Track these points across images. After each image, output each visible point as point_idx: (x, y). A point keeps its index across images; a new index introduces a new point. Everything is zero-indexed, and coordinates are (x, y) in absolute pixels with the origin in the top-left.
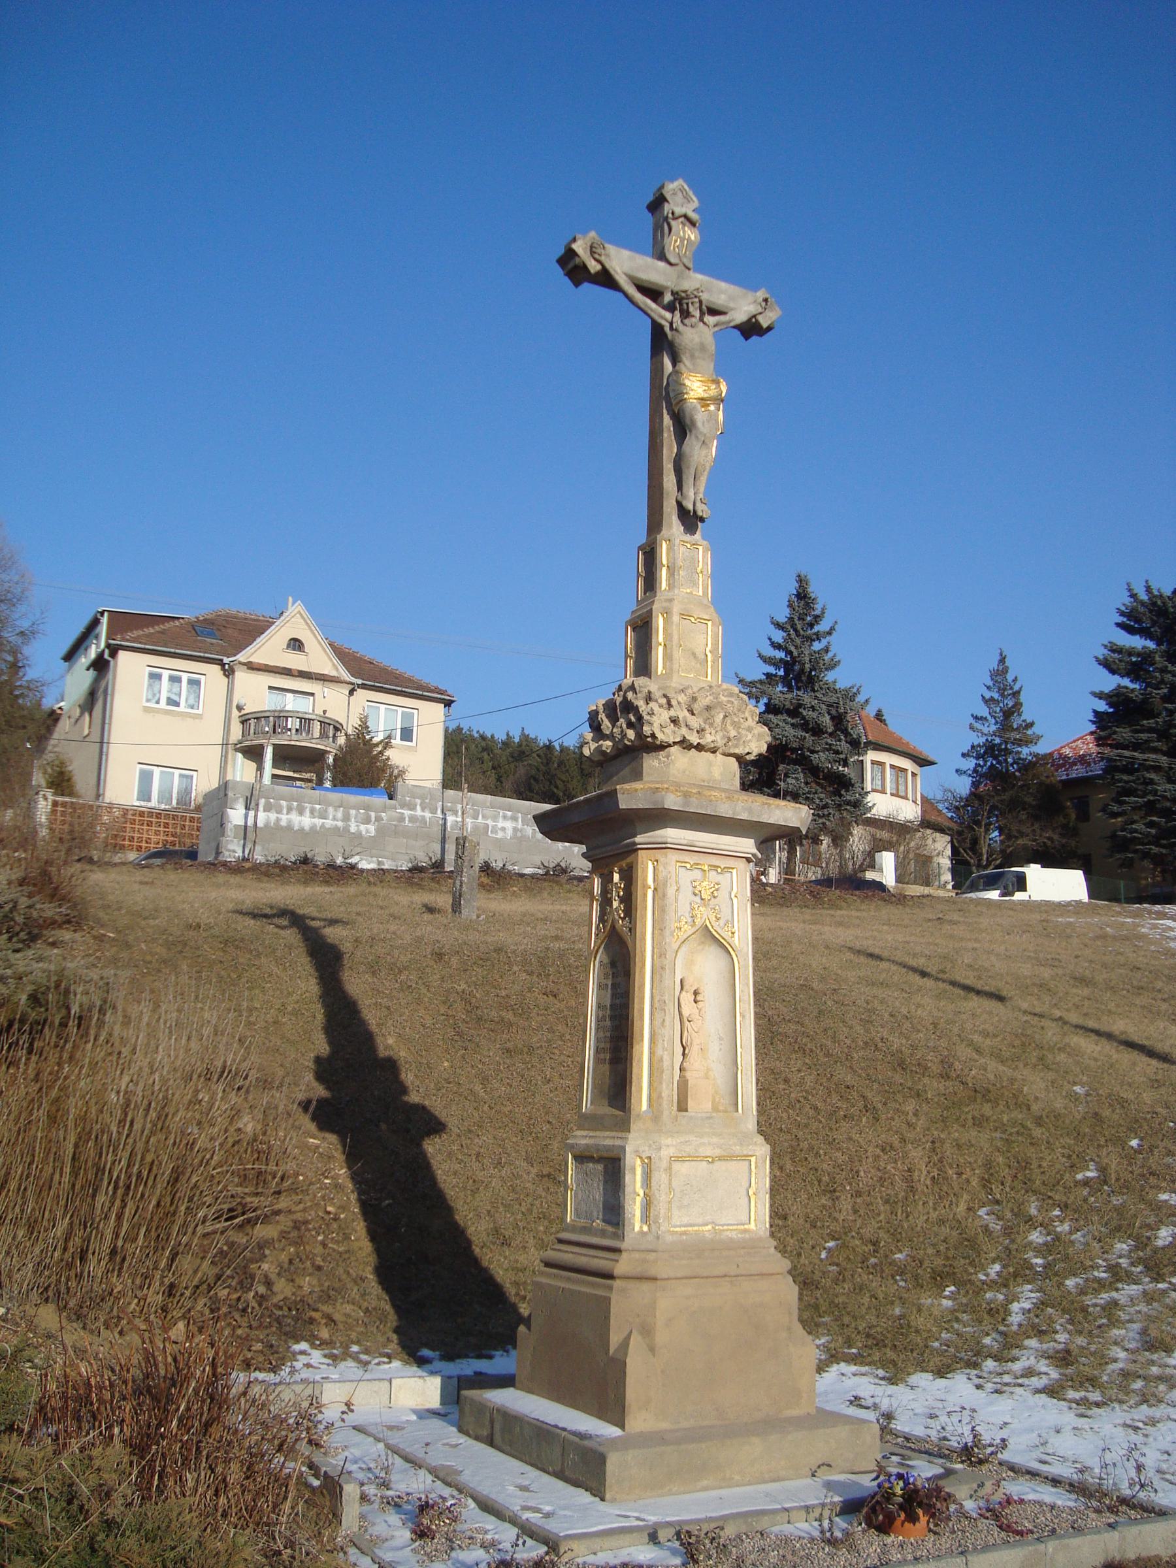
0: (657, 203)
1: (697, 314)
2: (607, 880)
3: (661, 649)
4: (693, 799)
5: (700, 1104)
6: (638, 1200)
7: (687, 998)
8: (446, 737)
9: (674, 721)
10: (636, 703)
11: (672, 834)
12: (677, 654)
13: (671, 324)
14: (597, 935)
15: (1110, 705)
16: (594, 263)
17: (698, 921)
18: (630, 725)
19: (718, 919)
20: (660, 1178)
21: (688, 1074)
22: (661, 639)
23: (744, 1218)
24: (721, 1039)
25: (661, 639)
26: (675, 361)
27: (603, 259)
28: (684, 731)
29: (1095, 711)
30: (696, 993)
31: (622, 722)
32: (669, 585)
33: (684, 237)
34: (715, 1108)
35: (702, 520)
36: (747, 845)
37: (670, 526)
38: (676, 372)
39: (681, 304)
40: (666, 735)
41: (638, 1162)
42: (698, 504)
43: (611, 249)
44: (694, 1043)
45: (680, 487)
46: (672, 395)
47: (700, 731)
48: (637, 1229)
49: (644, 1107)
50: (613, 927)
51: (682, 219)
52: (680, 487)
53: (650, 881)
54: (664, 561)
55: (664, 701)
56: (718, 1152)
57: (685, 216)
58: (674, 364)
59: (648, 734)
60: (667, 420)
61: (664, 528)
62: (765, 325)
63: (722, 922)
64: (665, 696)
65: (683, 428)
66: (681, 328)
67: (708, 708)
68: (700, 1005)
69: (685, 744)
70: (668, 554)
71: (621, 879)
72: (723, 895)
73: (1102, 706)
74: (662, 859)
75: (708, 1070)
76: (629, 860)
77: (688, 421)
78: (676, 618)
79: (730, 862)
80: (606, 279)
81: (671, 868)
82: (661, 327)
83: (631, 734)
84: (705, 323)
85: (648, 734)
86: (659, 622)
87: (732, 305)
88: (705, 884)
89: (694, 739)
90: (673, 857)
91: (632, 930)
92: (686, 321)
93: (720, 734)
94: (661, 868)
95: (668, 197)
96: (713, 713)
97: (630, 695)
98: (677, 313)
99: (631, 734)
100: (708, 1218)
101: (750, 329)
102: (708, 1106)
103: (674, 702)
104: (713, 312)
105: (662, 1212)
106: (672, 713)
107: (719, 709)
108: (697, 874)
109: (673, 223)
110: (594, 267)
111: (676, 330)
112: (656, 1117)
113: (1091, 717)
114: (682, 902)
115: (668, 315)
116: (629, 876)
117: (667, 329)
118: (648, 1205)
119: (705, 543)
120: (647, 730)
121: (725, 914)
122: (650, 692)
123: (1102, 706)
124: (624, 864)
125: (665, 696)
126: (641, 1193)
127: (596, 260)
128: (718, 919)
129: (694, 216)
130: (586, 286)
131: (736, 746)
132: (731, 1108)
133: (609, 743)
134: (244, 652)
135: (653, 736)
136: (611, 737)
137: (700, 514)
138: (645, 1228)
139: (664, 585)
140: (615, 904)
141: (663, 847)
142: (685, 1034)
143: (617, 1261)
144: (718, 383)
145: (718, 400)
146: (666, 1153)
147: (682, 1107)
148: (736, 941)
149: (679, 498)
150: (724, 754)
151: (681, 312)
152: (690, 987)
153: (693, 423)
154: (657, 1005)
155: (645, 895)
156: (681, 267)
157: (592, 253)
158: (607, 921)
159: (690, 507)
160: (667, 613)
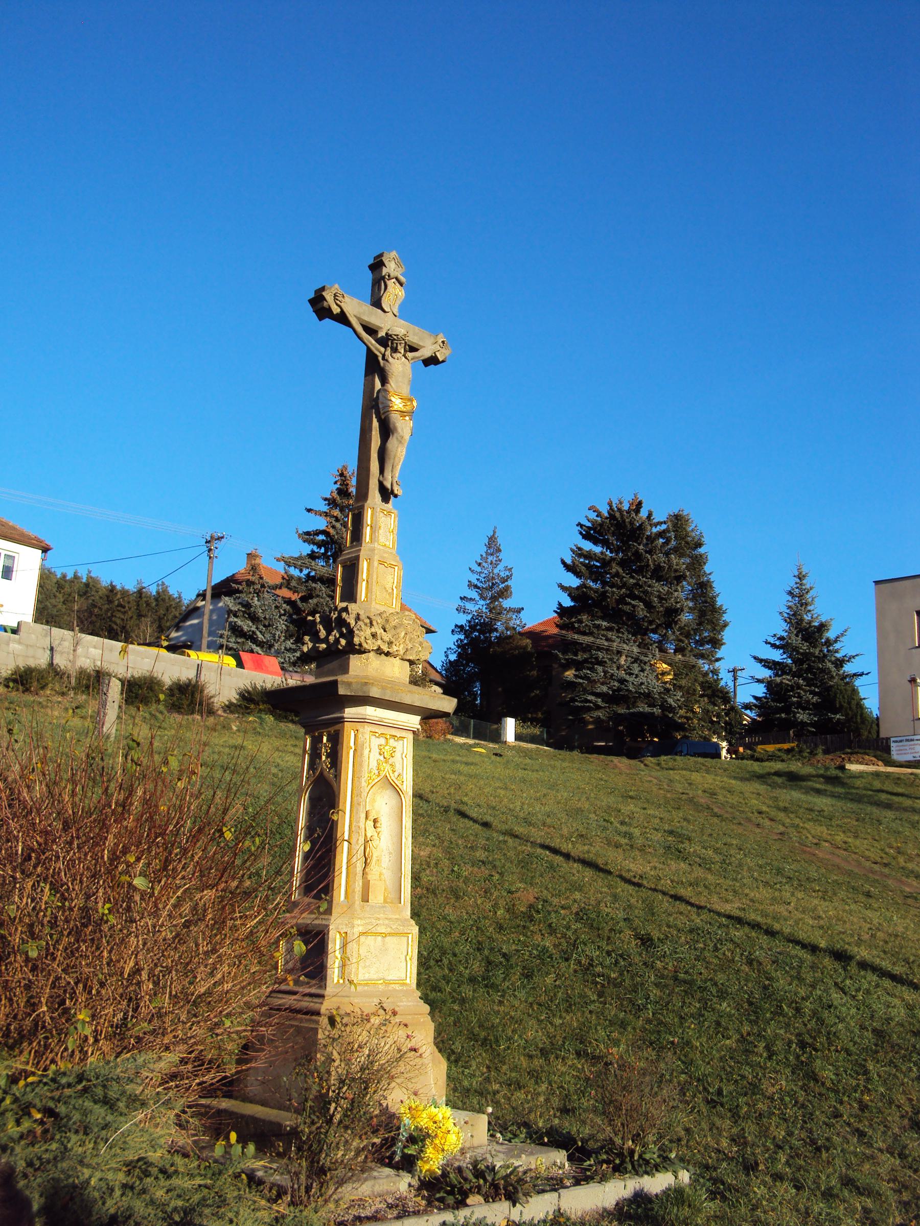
0: (377, 265)
1: (402, 351)
2: (316, 741)
3: (364, 583)
4: (388, 691)
5: (377, 897)
6: (337, 962)
7: (370, 823)
8: (41, 587)
9: (374, 636)
10: (348, 621)
11: (370, 711)
12: (375, 588)
13: (384, 356)
14: (307, 778)
15: (573, 599)
16: (336, 307)
17: (383, 774)
18: (342, 635)
19: (394, 772)
20: (352, 947)
21: (369, 877)
22: (365, 577)
23: (403, 976)
24: (390, 853)
25: (365, 577)
26: (384, 381)
27: (342, 305)
28: (379, 642)
29: (560, 604)
30: (375, 821)
31: (335, 633)
32: (371, 539)
33: (394, 295)
34: (385, 901)
35: (396, 496)
36: (414, 721)
37: (374, 498)
38: (384, 390)
39: (392, 343)
40: (370, 645)
41: (338, 936)
42: (395, 484)
43: (347, 299)
44: (374, 856)
45: (382, 471)
46: (381, 406)
47: (390, 643)
48: (335, 981)
49: (342, 898)
50: (321, 773)
51: (394, 280)
52: (382, 471)
53: (352, 744)
54: (369, 523)
55: (368, 621)
56: (389, 930)
57: (397, 279)
58: (383, 384)
59: (357, 643)
60: (375, 424)
61: (369, 499)
62: (441, 360)
63: (396, 774)
64: (368, 618)
65: (387, 431)
66: (390, 359)
67: (395, 628)
68: (379, 830)
69: (379, 651)
70: (372, 518)
71: (328, 740)
72: (398, 755)
73: (568, 602)
74: (361, 730)
75: (381, 874)
76: (337, 727)
77: (391, 426)
78: (376, 563)
79: (404, 734)
80: (342, 318)
81: (367, 736)
82: (376, 356)
83: (343, 642)
84: (406, 358)
85: (357, 643)
86: (364, 565)
87: (421, 344)
88: (387, 748)
89: (385, 648)
90: (368, 728)
91: (337, 776)
92: (394, 355)
93: (402, 646)
94: (360, 736)
95: (386, 263)
96: (398, 631)
97: (344, 615)
98: (389, 349)
99: (343, 642)
100: (381, 976)
101: (431, 361)
102: (381, 899)
103: (374, 623)
104: (413, 349)
105: (353, 970)
106: (373, 630)
107: (402, 629)
108: (382, 741)
109: (389, 283)
110: (336, 310)
111: (387, 361)
112: (351, 906)
113: (555, 607)
114: (371, 758)
115: (382, 349)
116: (336, 740)
117: (380, 358)
118: (343, 966)
119: (396, 512)
120: (356, 640)
121: (398, 767)
122: (358, 614)
123: (568, 602)
124: (332, 730)
125: (368, 618)
126: (339, 957)
127: (337, 305)
128: (394, 772)
129: (402, 279)
130: (327, 321)
131: (411, 655)
132: (397, 901)
133: (324, 646)
134: (410, 878)
135: (360, 645)
136: (326, 640)
137: (396, 492)
138: (341, 981)
139: (368, 539)
140: (324, 758)
141: (363, 721)
142: (368, 849)
143: (322, 1003)
144: (411, 400)
145: (411, 413)
146: (357, 930)
147: (365, 899)
148: (404, 788)
149: (381, 479)
150: (402, 659)
151: (392, 348)
152: (372, 817)
153: (395, 429)
154: (353, 829)
155: (348, 753)
156: (390, 314)
157: (335, 299)
158: (316, 769)
159: (389, 486)
160: (370, 560)
